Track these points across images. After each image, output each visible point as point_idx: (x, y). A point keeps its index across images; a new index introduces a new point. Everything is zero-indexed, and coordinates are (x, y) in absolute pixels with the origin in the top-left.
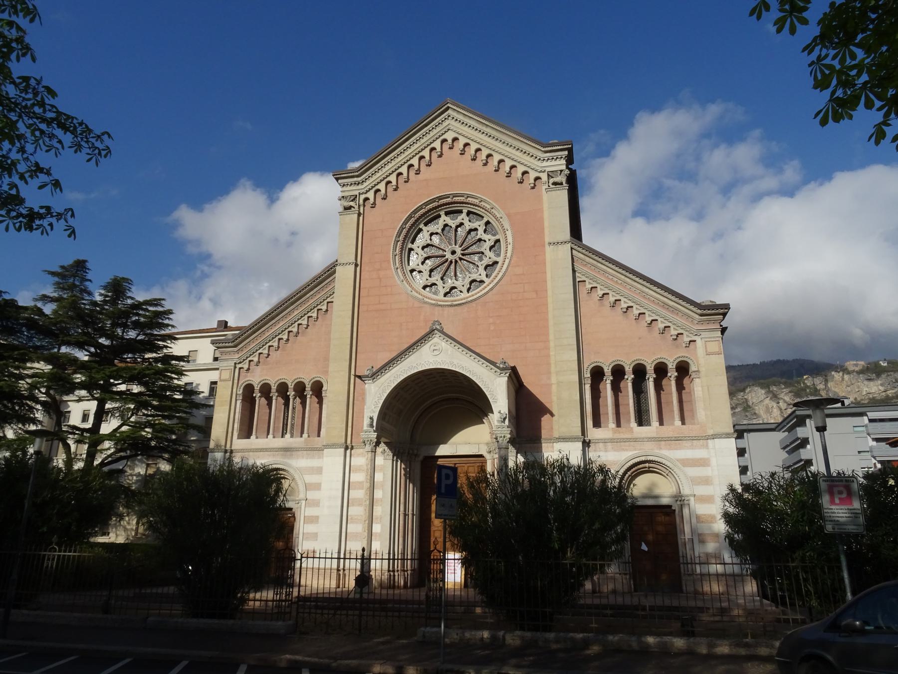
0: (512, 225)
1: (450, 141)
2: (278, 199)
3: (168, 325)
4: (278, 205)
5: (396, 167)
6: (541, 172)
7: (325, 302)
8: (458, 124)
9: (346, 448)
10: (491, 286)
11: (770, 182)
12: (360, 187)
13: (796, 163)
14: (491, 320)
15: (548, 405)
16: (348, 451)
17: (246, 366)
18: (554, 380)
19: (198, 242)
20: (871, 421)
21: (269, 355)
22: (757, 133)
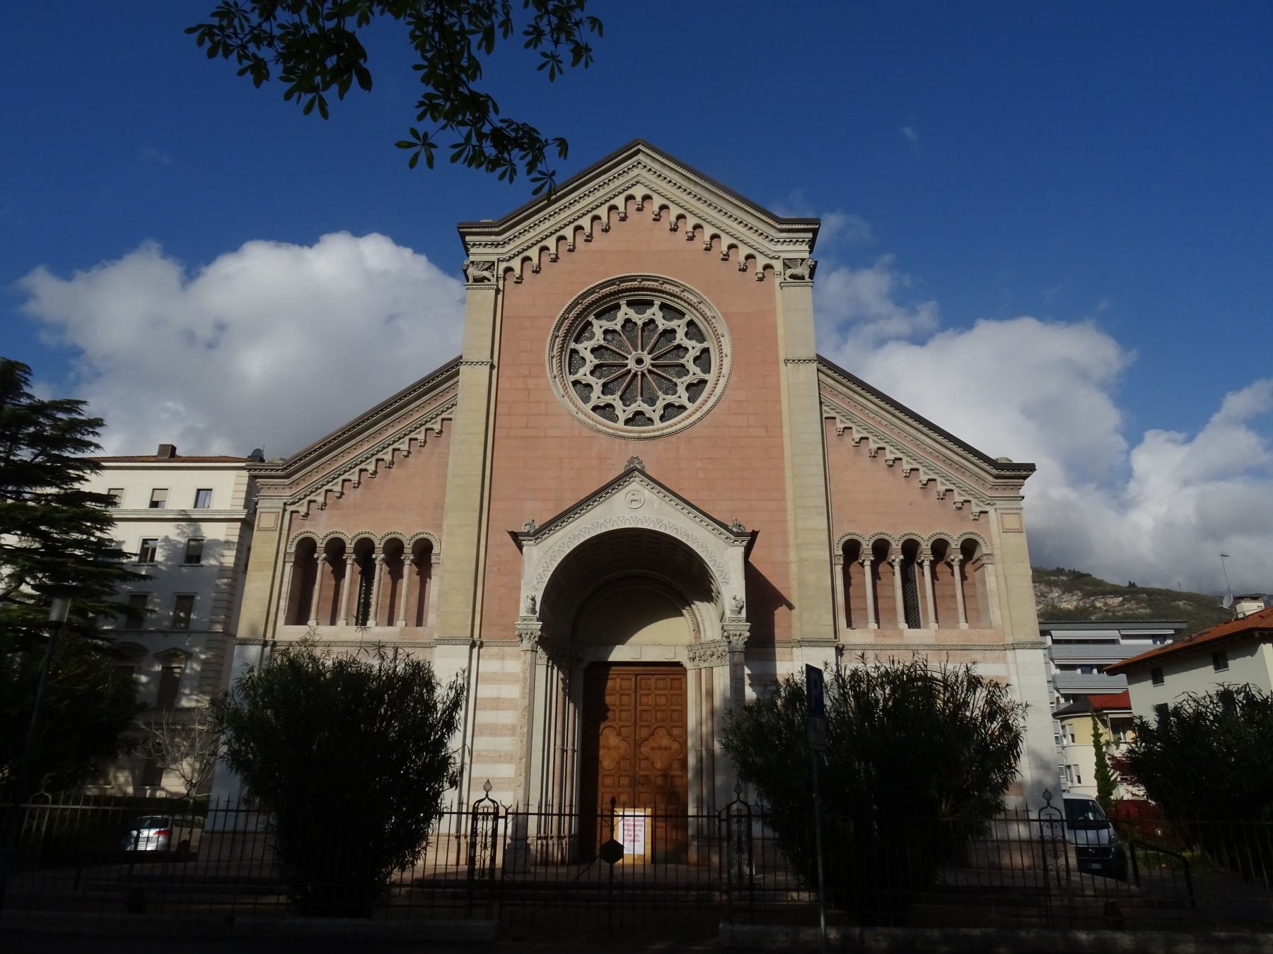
0: (732, 329)
1: (639, 199)
2: (198, 275)
3: (89, 444)
4: (201, 282)
5: (556, 227)
6: (773, 258)
7: (439, 418)
8: (647, 176)
9: (473, 645)
10: (698, 415)
11: (898, 324)
12: (500, 250)
13: (933, 303)
14: (699, 464)
15: (783, 592)
16: (475, 650)
17: (303, 510)
18: (793, 556)
19: (60, 328)
20: (1055, 642)
21: (342, 494)
22: (887, 258)
